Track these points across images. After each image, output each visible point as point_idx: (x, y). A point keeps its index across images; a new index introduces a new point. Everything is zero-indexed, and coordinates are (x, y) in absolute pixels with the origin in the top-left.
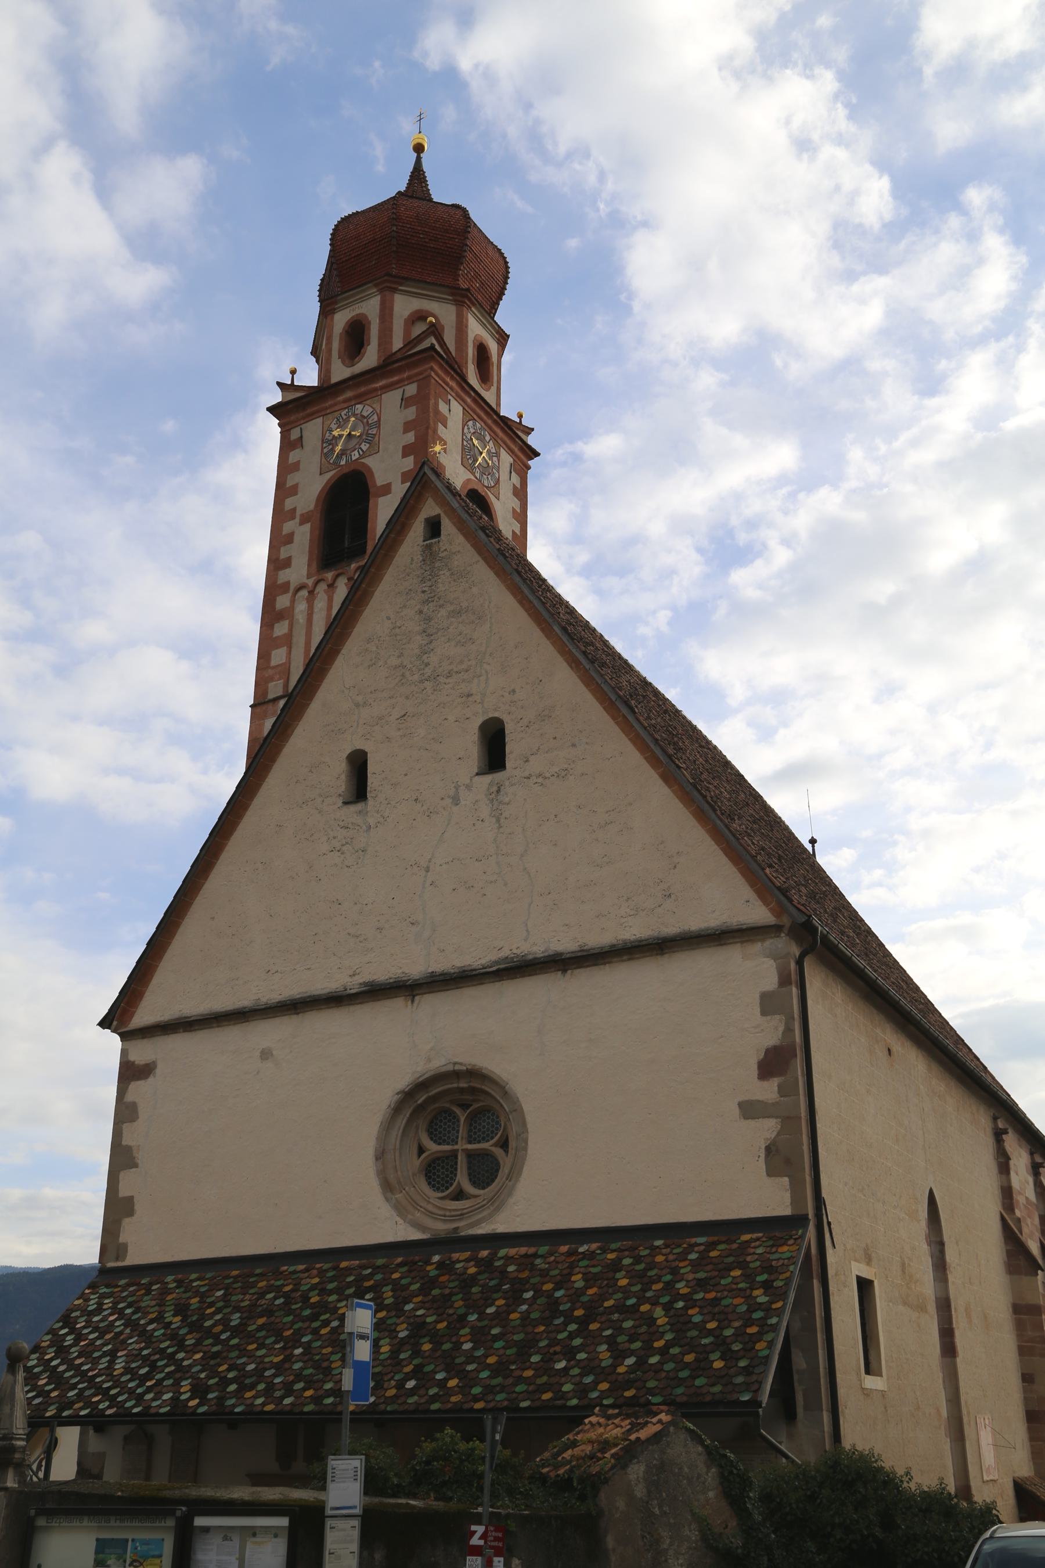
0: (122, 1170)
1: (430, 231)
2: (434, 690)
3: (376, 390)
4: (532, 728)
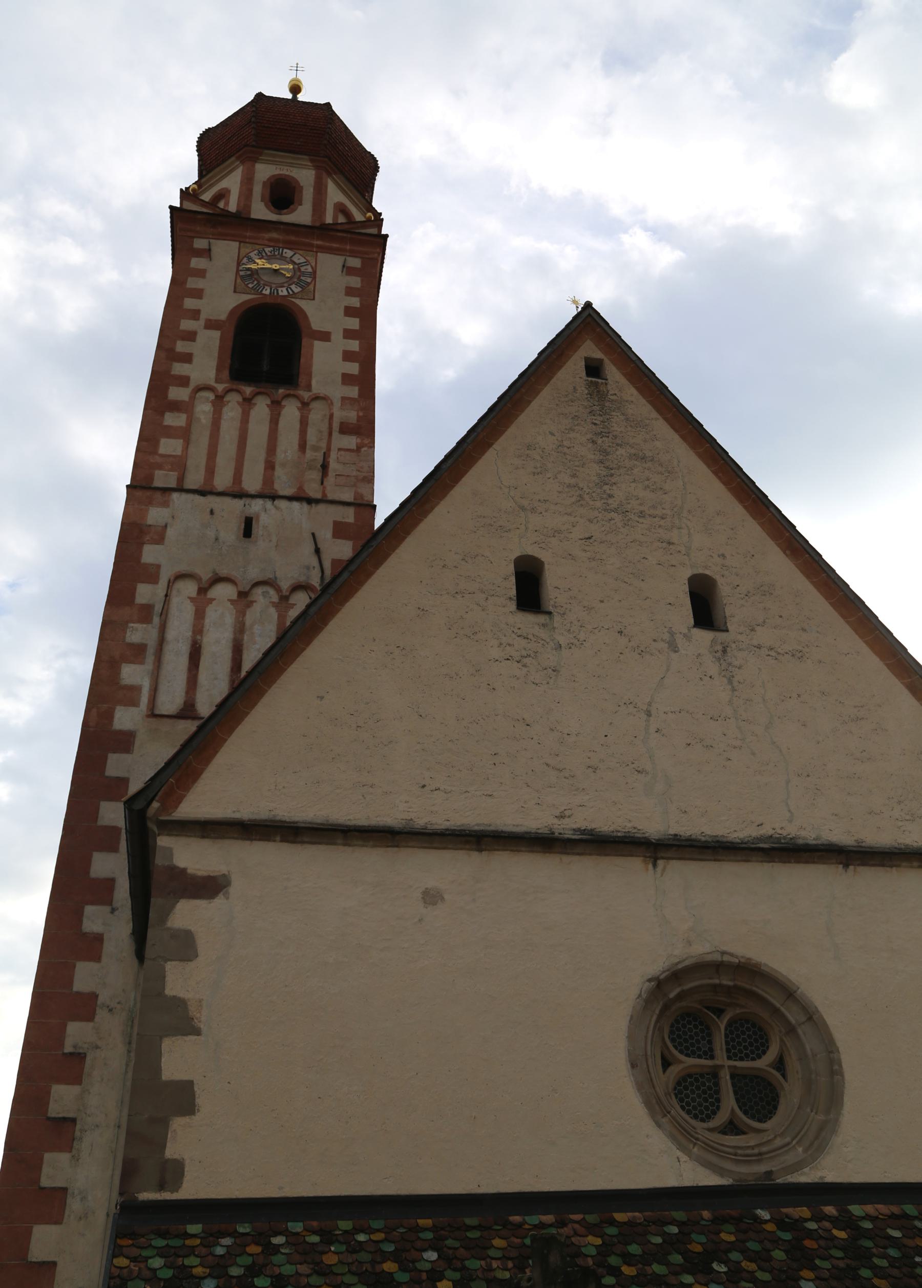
0: (167, 1036)
3: (312, 245)
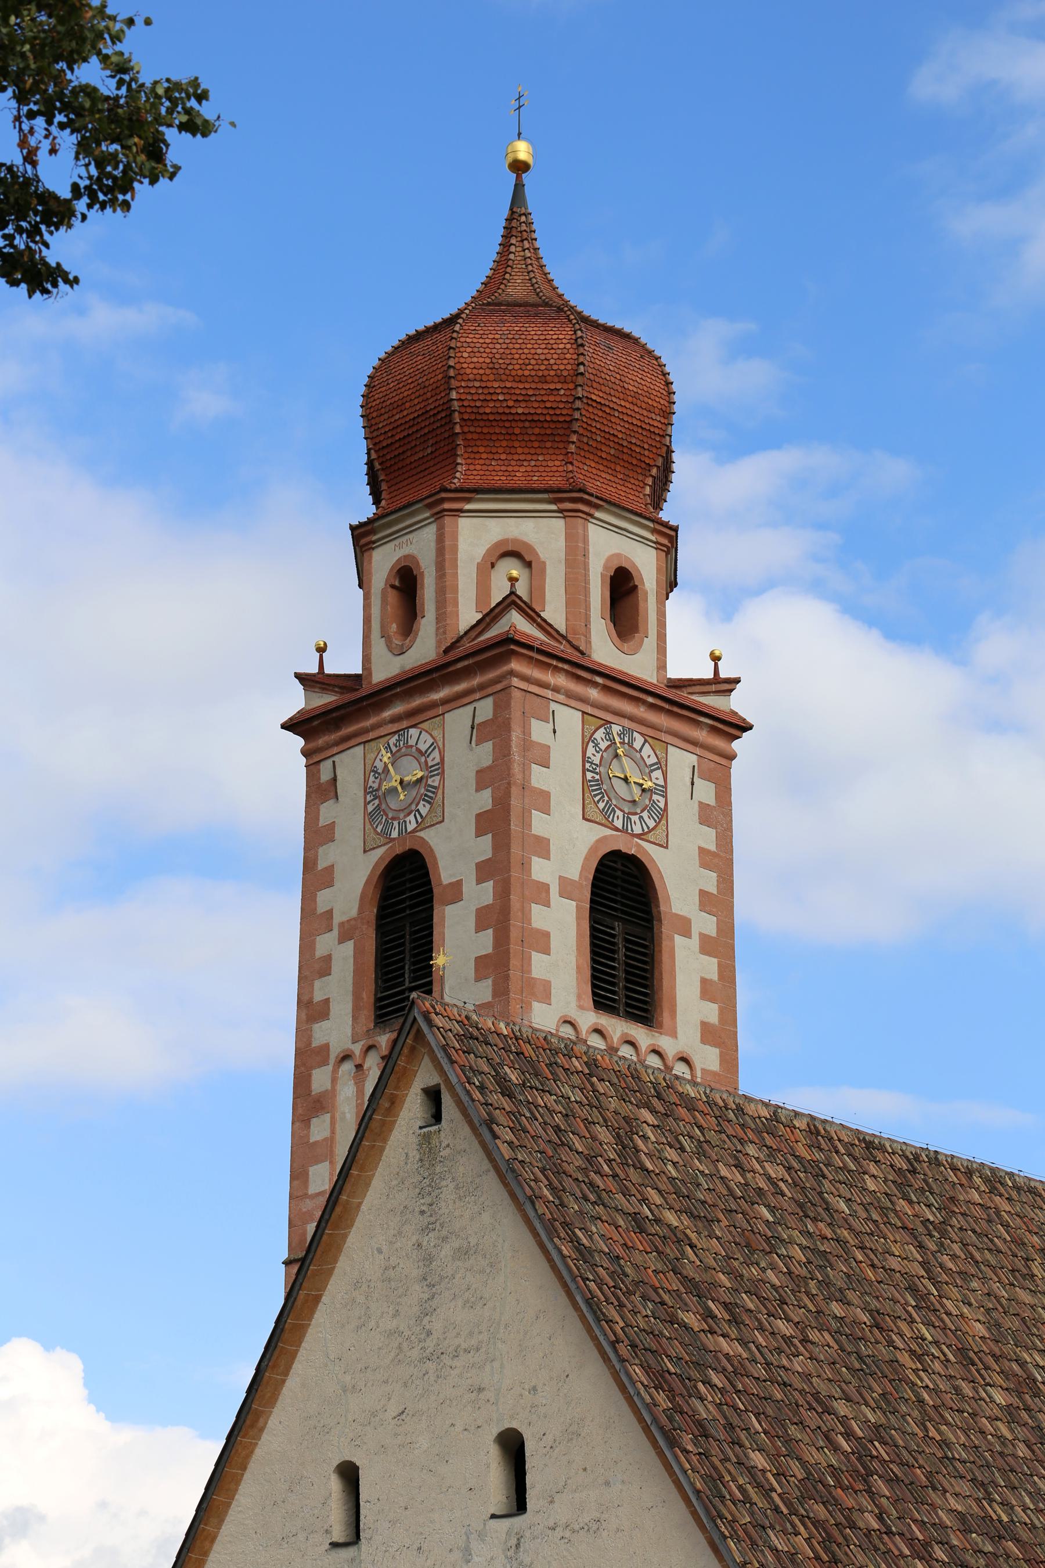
1: (515, 385)
2: (438, 1377)
3: (434, 705)
4: (557, 1450)
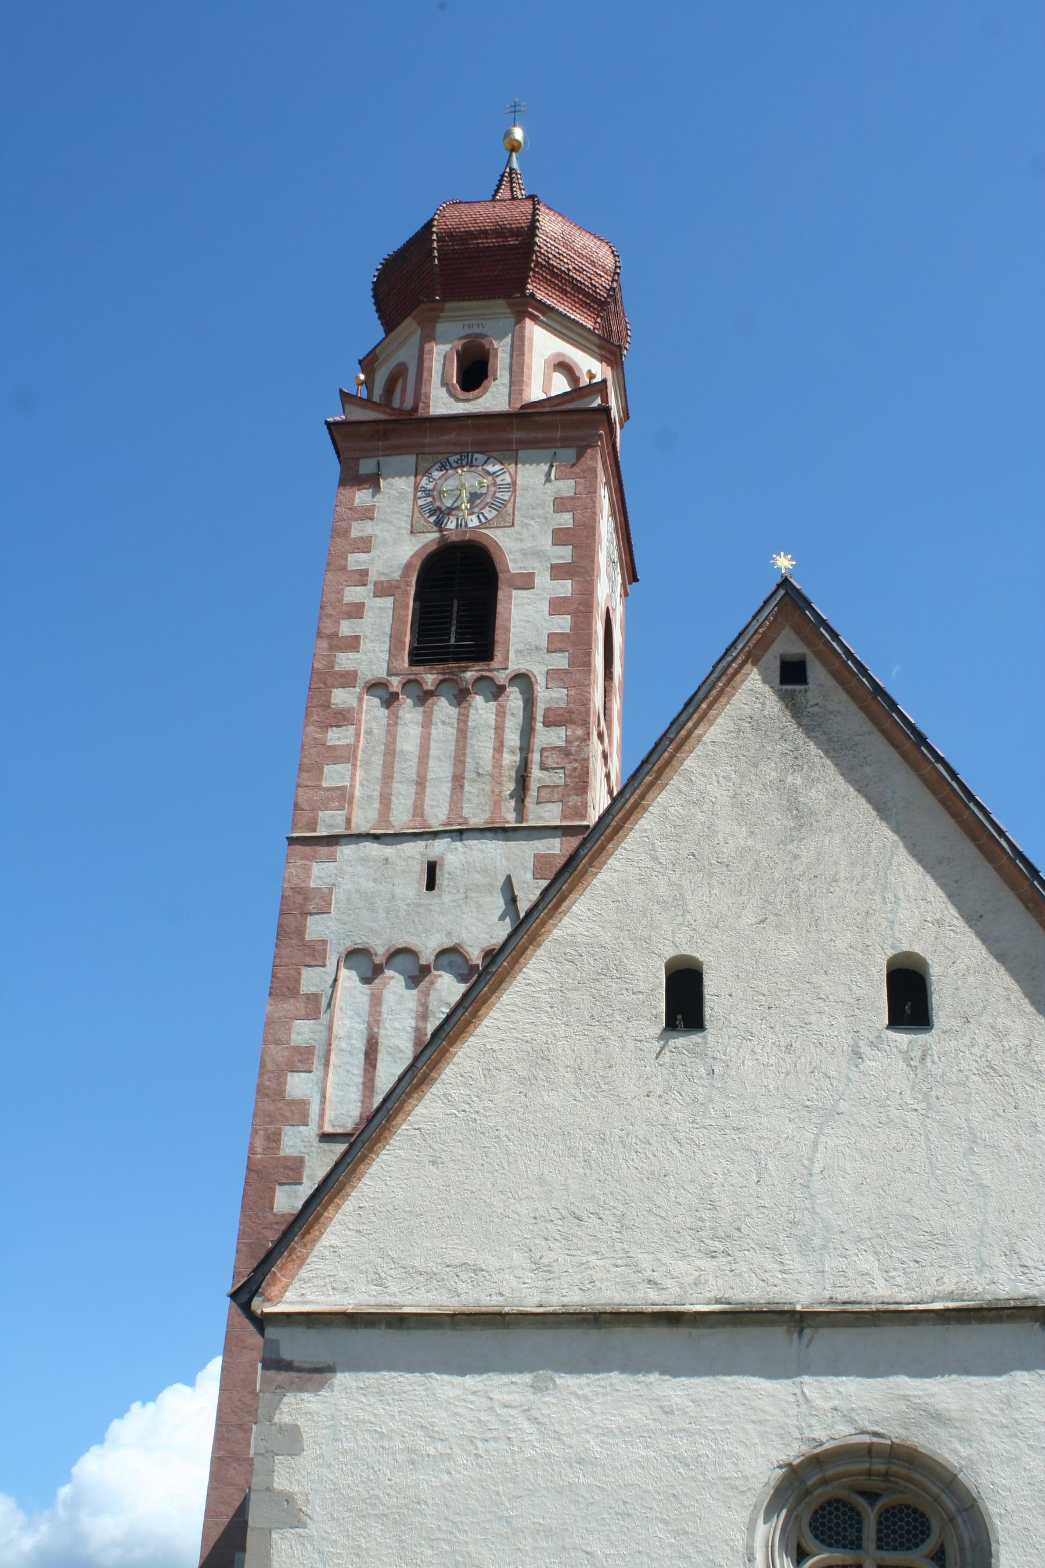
3: (509, 442)
